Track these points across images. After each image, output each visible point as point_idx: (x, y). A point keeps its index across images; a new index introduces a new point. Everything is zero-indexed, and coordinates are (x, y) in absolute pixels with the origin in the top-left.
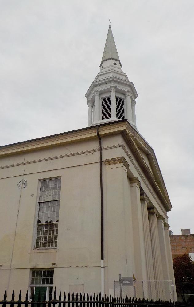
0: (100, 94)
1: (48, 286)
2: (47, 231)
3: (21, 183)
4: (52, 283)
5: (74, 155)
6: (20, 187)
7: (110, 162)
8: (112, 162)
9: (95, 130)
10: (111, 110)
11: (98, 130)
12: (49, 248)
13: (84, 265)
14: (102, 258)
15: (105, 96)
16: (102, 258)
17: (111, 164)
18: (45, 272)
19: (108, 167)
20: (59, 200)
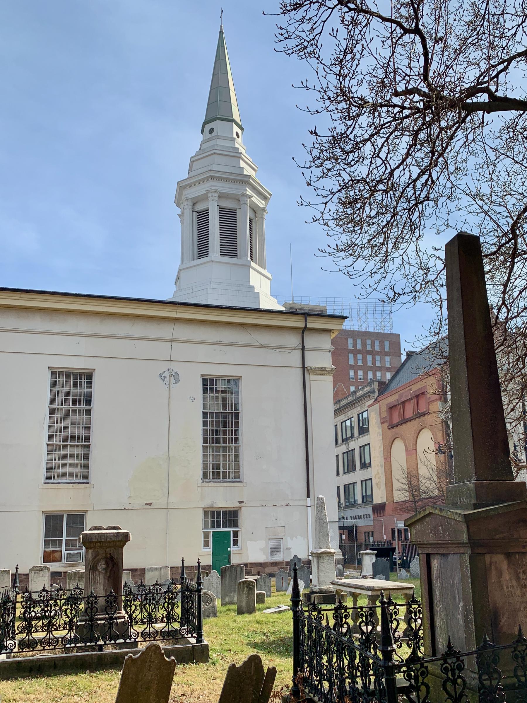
0: (194, 204)
1: (231, 530)
2: (219, 455)
3: (167, 374)
4: (236, 525)
5: (262, 346)
6: (167, 380)
7: (317, 372)
8: (320, 372)
9: (302, 318)
10: (209, 248)
11: (306, 321)
12: (225, 480)
13: (284, 503)
14: (308, 496)
15: (200, 207)
16: (308, 496)
17: (317, 374)
18: (213, 512)
19: (313, 377)
20: (337, 412)
